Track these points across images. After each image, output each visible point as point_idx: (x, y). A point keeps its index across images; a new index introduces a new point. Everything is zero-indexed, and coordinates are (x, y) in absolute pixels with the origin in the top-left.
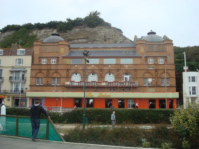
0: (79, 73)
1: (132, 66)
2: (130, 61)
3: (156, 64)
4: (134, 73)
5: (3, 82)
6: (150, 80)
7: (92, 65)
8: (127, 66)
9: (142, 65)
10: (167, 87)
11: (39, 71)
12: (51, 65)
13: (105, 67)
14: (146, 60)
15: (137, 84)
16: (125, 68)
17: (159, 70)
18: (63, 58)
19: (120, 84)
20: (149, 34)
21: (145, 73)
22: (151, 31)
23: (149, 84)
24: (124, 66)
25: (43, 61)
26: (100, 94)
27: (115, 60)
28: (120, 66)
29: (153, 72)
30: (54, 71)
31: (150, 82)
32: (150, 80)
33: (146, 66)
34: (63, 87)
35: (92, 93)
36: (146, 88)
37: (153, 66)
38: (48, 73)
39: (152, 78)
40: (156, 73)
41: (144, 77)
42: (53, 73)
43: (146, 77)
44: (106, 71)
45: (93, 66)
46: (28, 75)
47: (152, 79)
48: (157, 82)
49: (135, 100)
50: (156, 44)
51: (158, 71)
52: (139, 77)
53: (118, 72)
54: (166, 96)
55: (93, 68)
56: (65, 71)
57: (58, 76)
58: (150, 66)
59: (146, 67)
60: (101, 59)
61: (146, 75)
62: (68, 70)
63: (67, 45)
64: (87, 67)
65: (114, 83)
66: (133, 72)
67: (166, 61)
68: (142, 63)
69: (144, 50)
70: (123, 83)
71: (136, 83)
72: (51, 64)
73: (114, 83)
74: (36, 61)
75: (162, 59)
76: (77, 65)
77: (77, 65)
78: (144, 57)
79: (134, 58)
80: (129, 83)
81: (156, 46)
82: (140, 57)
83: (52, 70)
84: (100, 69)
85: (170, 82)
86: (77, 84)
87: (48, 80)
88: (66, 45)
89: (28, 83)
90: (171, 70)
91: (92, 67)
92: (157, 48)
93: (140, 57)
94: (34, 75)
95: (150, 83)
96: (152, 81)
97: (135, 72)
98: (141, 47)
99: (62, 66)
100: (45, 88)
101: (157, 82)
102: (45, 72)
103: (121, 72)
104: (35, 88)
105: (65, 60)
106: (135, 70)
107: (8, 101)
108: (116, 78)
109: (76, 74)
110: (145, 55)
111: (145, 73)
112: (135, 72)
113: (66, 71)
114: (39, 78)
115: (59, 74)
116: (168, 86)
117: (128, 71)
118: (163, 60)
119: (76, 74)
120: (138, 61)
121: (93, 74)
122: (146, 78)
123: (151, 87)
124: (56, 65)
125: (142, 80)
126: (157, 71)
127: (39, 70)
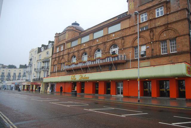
3: (151, 20)
6: (144, 48)
8: (114, 35)
15: (122, 57)
17: (126, 36)
19: (69, 66)
20: (73, 24)
22: (76, 22)
27: (102, 31)
30: (164, 28)
32: (144, 48)
38: (151, 34)
44: (94, 48)
45: (84, 45)
51: (91, 48)
52: (127, 46)
54: (139, 74)
57: (172, 34)
67: (168, 8)
68: (131, 25)
72: (155, 19)
75: (145, 15)
78: (133, 15)
86: (101, 62)
87: (153, 48)
88: (71, 30)
89: (50, 72)
90: (180, 20)
101: (153, 50)
103: (108, 45)
104: (53, 74)
107: (82, 94)
113: (67, 55)
114: (55, 65)
115: (175, 31)
118: (163, 10)
124: (166, 17)
127: (164, 25)
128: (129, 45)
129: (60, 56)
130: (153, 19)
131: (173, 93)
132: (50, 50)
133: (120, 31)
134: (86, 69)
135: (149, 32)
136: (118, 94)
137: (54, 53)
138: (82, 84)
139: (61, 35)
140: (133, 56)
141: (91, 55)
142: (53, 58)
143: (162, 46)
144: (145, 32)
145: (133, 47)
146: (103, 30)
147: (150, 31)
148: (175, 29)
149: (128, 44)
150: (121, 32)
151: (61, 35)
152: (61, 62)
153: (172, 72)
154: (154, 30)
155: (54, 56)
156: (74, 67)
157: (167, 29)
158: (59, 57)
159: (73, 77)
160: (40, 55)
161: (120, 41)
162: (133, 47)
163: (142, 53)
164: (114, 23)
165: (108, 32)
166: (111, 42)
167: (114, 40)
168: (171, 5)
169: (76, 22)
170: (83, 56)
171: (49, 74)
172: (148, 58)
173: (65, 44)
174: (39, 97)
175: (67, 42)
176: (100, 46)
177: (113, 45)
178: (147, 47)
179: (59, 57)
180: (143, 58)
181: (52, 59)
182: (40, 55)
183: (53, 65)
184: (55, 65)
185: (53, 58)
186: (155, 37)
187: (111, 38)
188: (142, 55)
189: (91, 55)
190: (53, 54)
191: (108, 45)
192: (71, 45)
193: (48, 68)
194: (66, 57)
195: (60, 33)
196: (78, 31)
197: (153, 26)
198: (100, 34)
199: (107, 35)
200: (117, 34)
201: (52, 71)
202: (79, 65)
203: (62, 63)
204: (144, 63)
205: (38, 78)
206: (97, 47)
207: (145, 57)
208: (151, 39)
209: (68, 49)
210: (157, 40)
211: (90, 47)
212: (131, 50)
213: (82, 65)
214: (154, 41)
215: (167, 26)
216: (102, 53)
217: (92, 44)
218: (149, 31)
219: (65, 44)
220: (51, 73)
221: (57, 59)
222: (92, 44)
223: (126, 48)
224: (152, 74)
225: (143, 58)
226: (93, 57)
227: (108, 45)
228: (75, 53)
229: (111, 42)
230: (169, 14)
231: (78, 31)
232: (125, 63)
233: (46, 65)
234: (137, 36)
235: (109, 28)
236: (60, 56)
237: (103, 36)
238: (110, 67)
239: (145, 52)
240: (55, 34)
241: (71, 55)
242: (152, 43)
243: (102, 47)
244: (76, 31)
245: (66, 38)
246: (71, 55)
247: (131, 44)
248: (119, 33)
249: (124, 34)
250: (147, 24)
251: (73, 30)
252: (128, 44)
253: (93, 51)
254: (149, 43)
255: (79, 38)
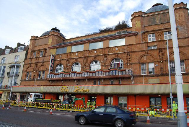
0: (100, 62)
1: (125, 48)
2: (122, 42)
3: (159, 41)
6: (151, 66)
7: (76, 52)
8: (117, 49)
9: (138, 45)
10: (145, 76)
14: (144, 38)
15: (128, 72)
16: (114, 51)
17: (132, 52)
19: (55, 76)
22: (56, 28)
23: (150, 72)
24: (114, 49)
27: (83, 46)
29: (156, 53)
30: (144, 53)
32: (151, 66)
33: (144, 46)
34: (47, 81)
36: (141, 78)
37: (155, 44)
38: (67, 63)
39: (154, 62)
45: (77, 54)
47: (155, 64)
48: (162, 68)
50: (158, 14)
51: (87, 58)
52: (133, 62)
53: (105, 59)
55: (77, 56)
58: (150, 45)
59: (144, 47)
63: (56, 35)
65: (97, 73)
66: (125, 56)
71: (127, 71)
73: (100, 73)
76: (61, 54)
77: (61, 54)
78: (140, 33)
80: (117, 72)
81: (159, 16)
82: (136, 34)
83: (39, 62)
85: (186, 68)
88: (55, 35)
89: (20, 78)
93: (136, 34)
94: (25, 70)
96: (156, 67)
97: (128, 56)
98: (137, 22)
101: (162, 68)
103: (110, 58)
106: (128, 53)
108: (102, 66)
109: (96, 63)
112: (128, 56)
114: (28, 72)
116: (146, 75)
119: (96, 63)
120: (133, 40)
121: (77, 65)
122: (145, 63)
123: (153, 76)
128: (136, 61)
130: (162, 41)
134: (80, 81)
135: (158, 52)
137: (29, 58)
138: (56, 95)
141: (86, 66)
142: (26, 64)
144: (154, 51)
148: (184, 53)
152: (40, 70)
153: (148, 90)
155: (28, 61)
158: (36, 63)
160: (18, 55)
163: (151, 70)
164: (118, 37)
165: (71, 51)
166: (144, 53)
167: (118, 54)
168: (180, 32)
169: (56, 28)
170: (57, 68)
172: (157, 76)
173: (46, 49)
177: (75, 62)
178: (156, 65)
179: (36, 63)
181: (24, 64)
182: (18, 55)
183: (26, 72)
185: (26, 64)
189: (86, 67)
190: (26, 58)
191: (109, 58)
195: (37, 37)
196: (62, 38)
198: (81, 48)
199: (71, 53)
202: (59, 77)
203: (41, 71)
204: (153, 80)
207: (152, 74)
208: (160, 58)
209: (66, 53)
212: (138, 66)
213: (63, 77)
214: (164, 61)
216: (82, 67)
219: (46, 49)
221: (33, 65)
224: (165, 91)
225: (150, 75)
226: (88, 68)
227: (110, 58)
228: (61, 61)
229: (114, 56)
230: (46, 56)
231: (62, 38)
238: (112, 80)
239: (153, 69)
242: (161, 62)
243: (64, 62)
245: (49, 43)
249: (129, 49)
251: (57, 36)
255: (87, 43)
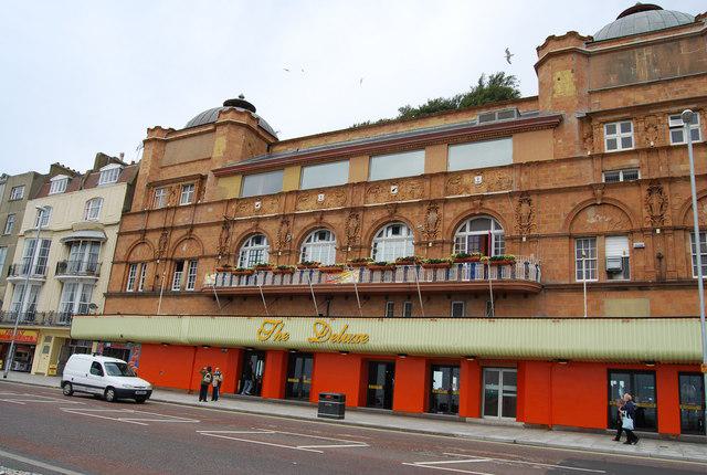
3: (650, 151)
4: (518, 211)
5: (97, 280)
6: (617, 249)
8: (478, 179)
10: (591, 287)
11: (138, 237)
12: (198, 208)
13: (371, 197)
17: (540, 192)
18: (221, 174)
19: (235, 279)
21: (580, 210)
25: (608, 137)
26: (269, 328)
28: (441, 182)
31: (615, 260)
32: (617, 249)
35: (285, 320)
39: (629, 234)
40: (655, 200)
41: (578, 230)
42: (180, 243)
43: (590, 230)
44: (376, 216)
45: (321, 197)
46: (106, 255)
48: (660, 258)
49: (433, 361)
52: (543, 231)
53: (433, 216)
56: (217, 230)
60: (517, 136)
61: (592, 219)
62: (225, 223)
64: (300, 206)
68: (565, 155)
69: (579, 84)
70: (448, 267)
71: (520, 266)
74: (139, 202)
75: (625, 129)
78: (572, 121)
79: (518, 131)
81: (647, 52)
84: (349, 206)
89: (103, 285)
91: (390, 196)
92: (655, 64)
93: (555, 124)
94: (122, 254)
95: (617, 265)
99: (210, 209)
100: (145, 303)
101: (660, 258)
102: (154, 239)
103: (450, 214)
104: (118, 303)
105: (223, 183)
106: (525, 196)
108: (418, 244)
109: (396, 231)
110: (583, 112)
111: (580, 210)
112: (525, 206)
113: (220, 228)
114: (134, 265)
116: (593, 284)
117: (488, 204)
120: (542, 147)
121: (322, 237)
122: (592, 238)
125: (562, 246)
126: (660, 191)
129: (173, 228)
130: (663, 148)
131: (272, 382)
132: (112, 197)
133: (511, 166)
134: (332, 301)
136: (253, 392)
137: (139, 210)
139: (179, 139)
140: (169, 284)
143: (579, 253)
145: (570, 236)
146: (424, 152)
147: (650, 192)
148: (632, 211)
149: (545, 223)
150: (514, 175)
151: (179, 139)
154: (361, 214)
155: (136, 224)
156: (227, 285)
157: (190, 238)
159: (269, 328)
161: (510, 207)
162: (570, 236)
167: (482, 198)
169: (241, 97)
171: (97, 298)
172: (642, 287)
173: (203, 178)
174: (66, 410)
175: (221, 174)
176: (330, 220)
178: (636, 244)
180: (615, 283)
181: (120, 234)
184: (134, 265)
186: (669, 212)
187: (467, 189)
188: (611, 273)
190: (126, 212)
192: (241, 191)
193: (91, 270)
194: (210, 240)
195: (172, 131)
197: (662, 172)
198: (338, 174)
199: (297, 192)
200: (489, 176)
201: (117, 289)
205: (24, 309)
206: (391, 216)
207: (620, 278)
209: (222, 202)
210: (679, 224)
211: (353, 210)
213: (227, 285)
214: (669, 228)
215: (318, 217)
216: (341, 249)
217: (366, 197)
218: (426, 207)
219: (203, 178)
220: (108, 296)
222: (366, 197)
223: (539, 237)
225: (615, 283)
232: (536, 294)
233: (86, 259)
234: (691, 198)
235: (306, 170)
236: (173, 228)
237: (423, 176)
239: (625, 260)
240: (538, 49)
241: (238, 230)
243: (271, 229)
244: (258, 135)
246: (238, 230)
247: (564, 227)
248: (505, 174)
250: (634, 162)
251: (248, 127)
252: (545, 223)
253: (234, 238)
254: (642, 231)
255: (235, 174)
